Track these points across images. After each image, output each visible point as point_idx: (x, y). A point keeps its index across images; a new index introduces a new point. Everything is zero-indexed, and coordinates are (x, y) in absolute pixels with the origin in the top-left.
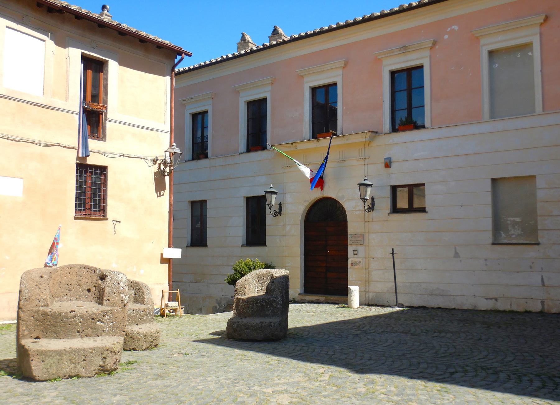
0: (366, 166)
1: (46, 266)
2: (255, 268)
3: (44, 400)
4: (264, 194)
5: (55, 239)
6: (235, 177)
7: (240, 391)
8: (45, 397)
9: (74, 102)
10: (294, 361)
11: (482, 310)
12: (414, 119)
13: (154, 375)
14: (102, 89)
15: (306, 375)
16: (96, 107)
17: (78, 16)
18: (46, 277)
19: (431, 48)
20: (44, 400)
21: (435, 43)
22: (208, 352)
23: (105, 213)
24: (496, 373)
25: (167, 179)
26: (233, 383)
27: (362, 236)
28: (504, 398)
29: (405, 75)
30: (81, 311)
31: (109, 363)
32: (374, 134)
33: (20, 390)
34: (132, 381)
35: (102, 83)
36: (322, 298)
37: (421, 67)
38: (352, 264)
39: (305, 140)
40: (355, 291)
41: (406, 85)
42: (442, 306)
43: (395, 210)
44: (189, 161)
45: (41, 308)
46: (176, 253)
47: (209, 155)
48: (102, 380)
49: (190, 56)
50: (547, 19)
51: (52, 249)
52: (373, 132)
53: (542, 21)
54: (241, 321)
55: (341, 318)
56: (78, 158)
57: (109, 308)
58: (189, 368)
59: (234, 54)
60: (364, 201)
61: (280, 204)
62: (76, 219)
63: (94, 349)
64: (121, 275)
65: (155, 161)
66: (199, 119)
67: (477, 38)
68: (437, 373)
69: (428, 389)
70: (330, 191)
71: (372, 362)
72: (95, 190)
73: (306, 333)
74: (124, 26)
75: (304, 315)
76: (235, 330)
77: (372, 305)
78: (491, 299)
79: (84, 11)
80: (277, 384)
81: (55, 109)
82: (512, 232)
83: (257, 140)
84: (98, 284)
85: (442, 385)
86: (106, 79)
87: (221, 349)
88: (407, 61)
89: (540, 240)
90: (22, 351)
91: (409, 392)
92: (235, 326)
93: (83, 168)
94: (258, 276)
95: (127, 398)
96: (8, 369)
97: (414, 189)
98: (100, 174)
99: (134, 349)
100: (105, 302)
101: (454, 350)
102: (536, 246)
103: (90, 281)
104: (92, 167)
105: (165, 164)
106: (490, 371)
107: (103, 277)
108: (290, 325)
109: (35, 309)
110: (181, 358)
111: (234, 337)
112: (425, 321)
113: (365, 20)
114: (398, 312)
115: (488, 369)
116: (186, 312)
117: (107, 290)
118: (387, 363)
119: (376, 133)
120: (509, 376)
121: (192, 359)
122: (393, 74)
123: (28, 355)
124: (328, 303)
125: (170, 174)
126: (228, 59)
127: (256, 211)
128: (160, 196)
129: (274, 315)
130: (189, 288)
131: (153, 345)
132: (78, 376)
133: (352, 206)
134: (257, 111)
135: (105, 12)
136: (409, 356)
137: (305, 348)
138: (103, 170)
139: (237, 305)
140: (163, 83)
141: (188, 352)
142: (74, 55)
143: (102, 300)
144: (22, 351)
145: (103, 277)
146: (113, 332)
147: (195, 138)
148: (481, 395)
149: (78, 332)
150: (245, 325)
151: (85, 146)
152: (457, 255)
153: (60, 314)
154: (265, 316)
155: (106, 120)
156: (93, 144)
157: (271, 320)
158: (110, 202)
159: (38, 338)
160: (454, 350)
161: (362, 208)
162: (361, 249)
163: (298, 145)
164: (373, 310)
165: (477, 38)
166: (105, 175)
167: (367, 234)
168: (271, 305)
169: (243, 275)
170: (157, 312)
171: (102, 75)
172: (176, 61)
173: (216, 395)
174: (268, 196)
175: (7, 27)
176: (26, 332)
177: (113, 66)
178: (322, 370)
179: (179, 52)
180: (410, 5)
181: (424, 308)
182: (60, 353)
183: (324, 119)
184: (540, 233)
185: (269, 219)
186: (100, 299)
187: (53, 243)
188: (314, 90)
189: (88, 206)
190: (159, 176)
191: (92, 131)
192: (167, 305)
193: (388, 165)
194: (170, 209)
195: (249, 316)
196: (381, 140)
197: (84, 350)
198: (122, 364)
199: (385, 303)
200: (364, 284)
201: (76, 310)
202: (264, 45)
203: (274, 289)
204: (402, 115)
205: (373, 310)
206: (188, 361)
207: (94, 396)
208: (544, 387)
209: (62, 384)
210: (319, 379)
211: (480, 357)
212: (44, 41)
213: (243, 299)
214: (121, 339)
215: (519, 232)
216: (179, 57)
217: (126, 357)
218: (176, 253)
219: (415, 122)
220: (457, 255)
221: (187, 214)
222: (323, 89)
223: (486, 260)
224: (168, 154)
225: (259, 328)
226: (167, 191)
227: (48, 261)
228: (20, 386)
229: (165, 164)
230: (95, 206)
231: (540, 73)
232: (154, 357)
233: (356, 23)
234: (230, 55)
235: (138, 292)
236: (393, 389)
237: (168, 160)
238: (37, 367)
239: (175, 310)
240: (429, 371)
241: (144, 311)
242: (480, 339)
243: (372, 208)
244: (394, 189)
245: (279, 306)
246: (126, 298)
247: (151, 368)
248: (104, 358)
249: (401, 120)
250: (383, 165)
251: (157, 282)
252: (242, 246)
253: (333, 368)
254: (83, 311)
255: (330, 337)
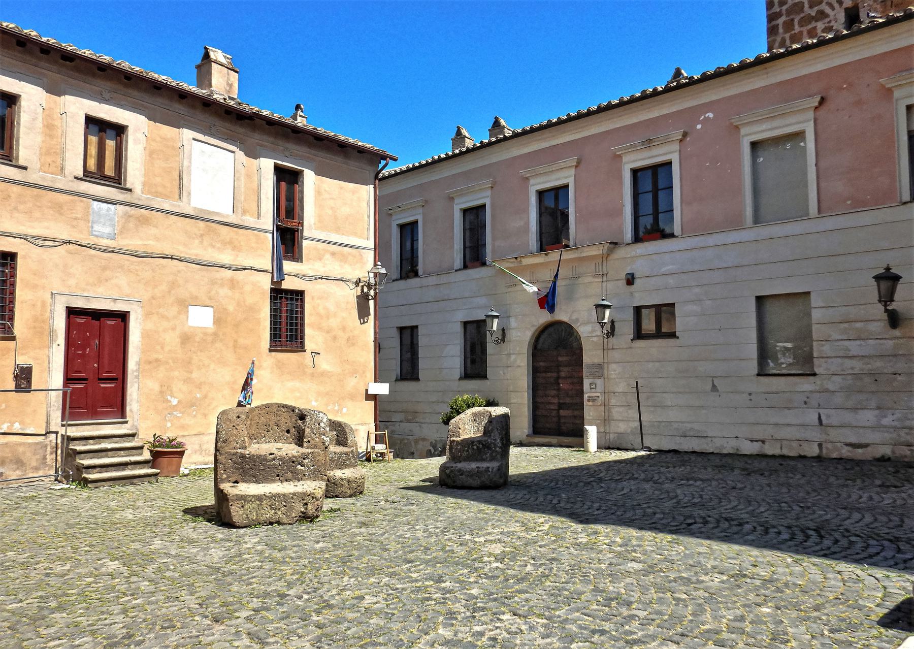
0: (604, 284)
1: (240, 404)
2: (473, 405)
3: (245, 546)
4: (484, 318)
5: (249, 374)
6: (448, 300)
7: (449, 540)
8: (246, 543)
9: (267, 221)
10: (512, 510)
11: (746, 455)
12: (662, 225)
13: (359, 523)
14: (297, 202)
15: (524, 524)
16: (290, 225)
17: (270, 122)
18: (243, 417)
19: (681, 141)
20: (245, 546)
21: (685, 135)
22: (417, 500)
23: (302, 343)
24: (740, 525)
25: (371, 303)
26: (442, 532)
27: (600, 366)
28: (740, 551)
29: (649, 173)
30: (280, 454)
31: (311, 509)
32: (612, 246)
33: (220, 536)
34: (335, 528)
35: (297, 195)
36: (554, 440)
37: (669, 164)
38: (588, 401)
39: (531, 254)
40: (592, 432)
41: (652, 182)
42: (697, 449)
43: (639, 335)
44: (397, 280)
45: (239, 451)
46: (383, 389)
47: (420, 273)
48: (304, 528)
49: (396, 160)
50: (822, 101)
51: (247, 384)
52: (611, 243)
53: (817, 104)
54: (454, 465)
55: (574, 463)
56: (273, 282)
57: (310, 451)
58: (396, 516)
59: (447, 154)
60: (602, 325)
61: (503, 330)
62: (270, 351)
63: (294, 494)
64: (321, 415)
65: (357, 283)
66: (409, 230)
67: (737, 127)
68: (672, 524)
69: (657, 540)
70: (562, 315)
71: (599, 512)
72: (292, 318)
73: (531, 480)
74: (321, 130)
75: (525, 460)
76: (448, 476)
77: (613, 449)
78: (757, 441)
79: (276, 116)
80: (490, 534)
81: (246, 228)
82: (782, 360)
83: (475, 255)
84: (297, 424)
85: (674, 536)
86: (302, 192)
87: (432, 497)
88: (652, 157)
89: (817, 370)
90: (221, 496)
91: (635, 543)
92: (448, 471)
93: (277, 293)
94: (474, 414)
95: (330, 545)
96: (206, 516)
97: (664, 311)
98: (297, 300)
99: (337, 497)
100: (305, 445)
101: (699, 500)
102: (811, 378)
103: (287, 421)
104: (287, 291)
105: (369, 286)
106: (735, 523)
107: (302, 417)
108: (512, 471)
109: (233, 451)
110: (388, 505)
111: (447, 484)
112: (674, 467)
113: (600, 110)
114: (643, 456)
115: (733, 520)
116: (396, 456)
117: (308, 431)
118: (618, 513)
119: (616, 244)
120: (755, 528)
121: (399, 507)
122: (635, 172)
123: (227, 500)
124: (561, 446)
125: (375, 298)
126: (440, 160)
127: (476, 337)
128: (364, 323)
129: (493, 459)
130: (398, 431)
131: (357, 490)
132: (279, 523)
133: (588, 332)
134: (474, 217)
135: (300, 113)
136: (645, 506)
137: (527, 497)
138: (300, 294)
139: (451, 448)
140: (365, 194)
141: (397, 500)
142: (267, 165)
143: (302, 442)
144: (221, 496)
145: (302, 417)
146: (315, 475)
147: (403, 251)
148: (715, 547)
149: (278, 476)
150: (460, 470)
151: (280, 269)
152: (714, 388)
153: (259, 456)
154: (483, 460)
155: (302, 238)
156: (289, 266)
157: (488, 465)
158: (308, 331)
159: (236, 482)
160: (699, 500)
161: (599, 333)
162: (599, 382)
163: (523, 260)
164: (614, 454)
165: (737, 127)
166: (302, 301)
167: (606, 365)
168: (489, 448)
169: (459, 413)
170: (362, 457)
171: (297, 186)
172: (380, 166)
173: (424, 544)
174: (488, 320)
175: (194, 139)
176: (225, 476)
177: (309, 177)
178: (542, 520)
179: (384, 157)
180: (655, 90)
181: (675, 451)
182: (260, 498)
183: (554, 228)
184: (816, 361)
185: (491, 348)
186: (300, 442)
187: (247, 379)
188: (541, 194)
189: (283, 337)
190: (363, 300)
191: (286, 252)
192: (373, 448)
193: (630, 280)
194: (375, 338)
195: (465, 460)
196: (621, 252)
197: (284, 495)
198: (324, 512)
199: (629, 446)
200: (604, 423)
201: (276, 452)
202: (481, 142)
203: (492, 430)
204: (647, 221)
205: (614, 454)
206: (395, 508)
207: (296, 542)
208: (791, 539)
209: (263, 531)
210: (538, 529)
211: (728, 507)
212: (233, 152)
213: (457, 441)
214: (323, 485)
215: (791, 360)
216: (383, 162)
217: (328, 504)
218: (383, 389)
219: (663, 230)
220: (714, 388)
221: (394, 343)
222: (553, 193)
223: (750, 394)
224: (372, 275)
225: (476, 473)
226: (372, 317)
227: (241, 399)
228: (221, 533)
229: (369, 286)
230: (291, 336)
231: (814, 168)
232: (359, 504)
233: (589, 113)
234: (443, 156)
235: (341, 433)
236: (618, 540)
237: (373, 282)
238: (237, 513)
239: (382, 454)
240: (664, 522)
241: (346, 454)
242: (734, 488)
243: (612, 332)
244: (638, 310)
245: (498, 449)
246: (327, 440)
247: (356, 516)
248: (306, 504)
249: (645, 228)
250: (625, 282)
251: (362, 424)
252: (461, 379)
253: (554, 518)
254: (283, 453)
255: (868, 546)
